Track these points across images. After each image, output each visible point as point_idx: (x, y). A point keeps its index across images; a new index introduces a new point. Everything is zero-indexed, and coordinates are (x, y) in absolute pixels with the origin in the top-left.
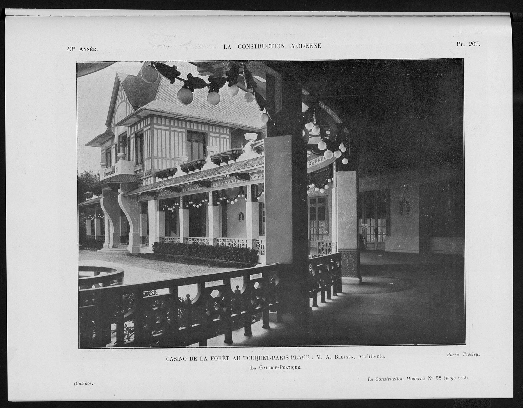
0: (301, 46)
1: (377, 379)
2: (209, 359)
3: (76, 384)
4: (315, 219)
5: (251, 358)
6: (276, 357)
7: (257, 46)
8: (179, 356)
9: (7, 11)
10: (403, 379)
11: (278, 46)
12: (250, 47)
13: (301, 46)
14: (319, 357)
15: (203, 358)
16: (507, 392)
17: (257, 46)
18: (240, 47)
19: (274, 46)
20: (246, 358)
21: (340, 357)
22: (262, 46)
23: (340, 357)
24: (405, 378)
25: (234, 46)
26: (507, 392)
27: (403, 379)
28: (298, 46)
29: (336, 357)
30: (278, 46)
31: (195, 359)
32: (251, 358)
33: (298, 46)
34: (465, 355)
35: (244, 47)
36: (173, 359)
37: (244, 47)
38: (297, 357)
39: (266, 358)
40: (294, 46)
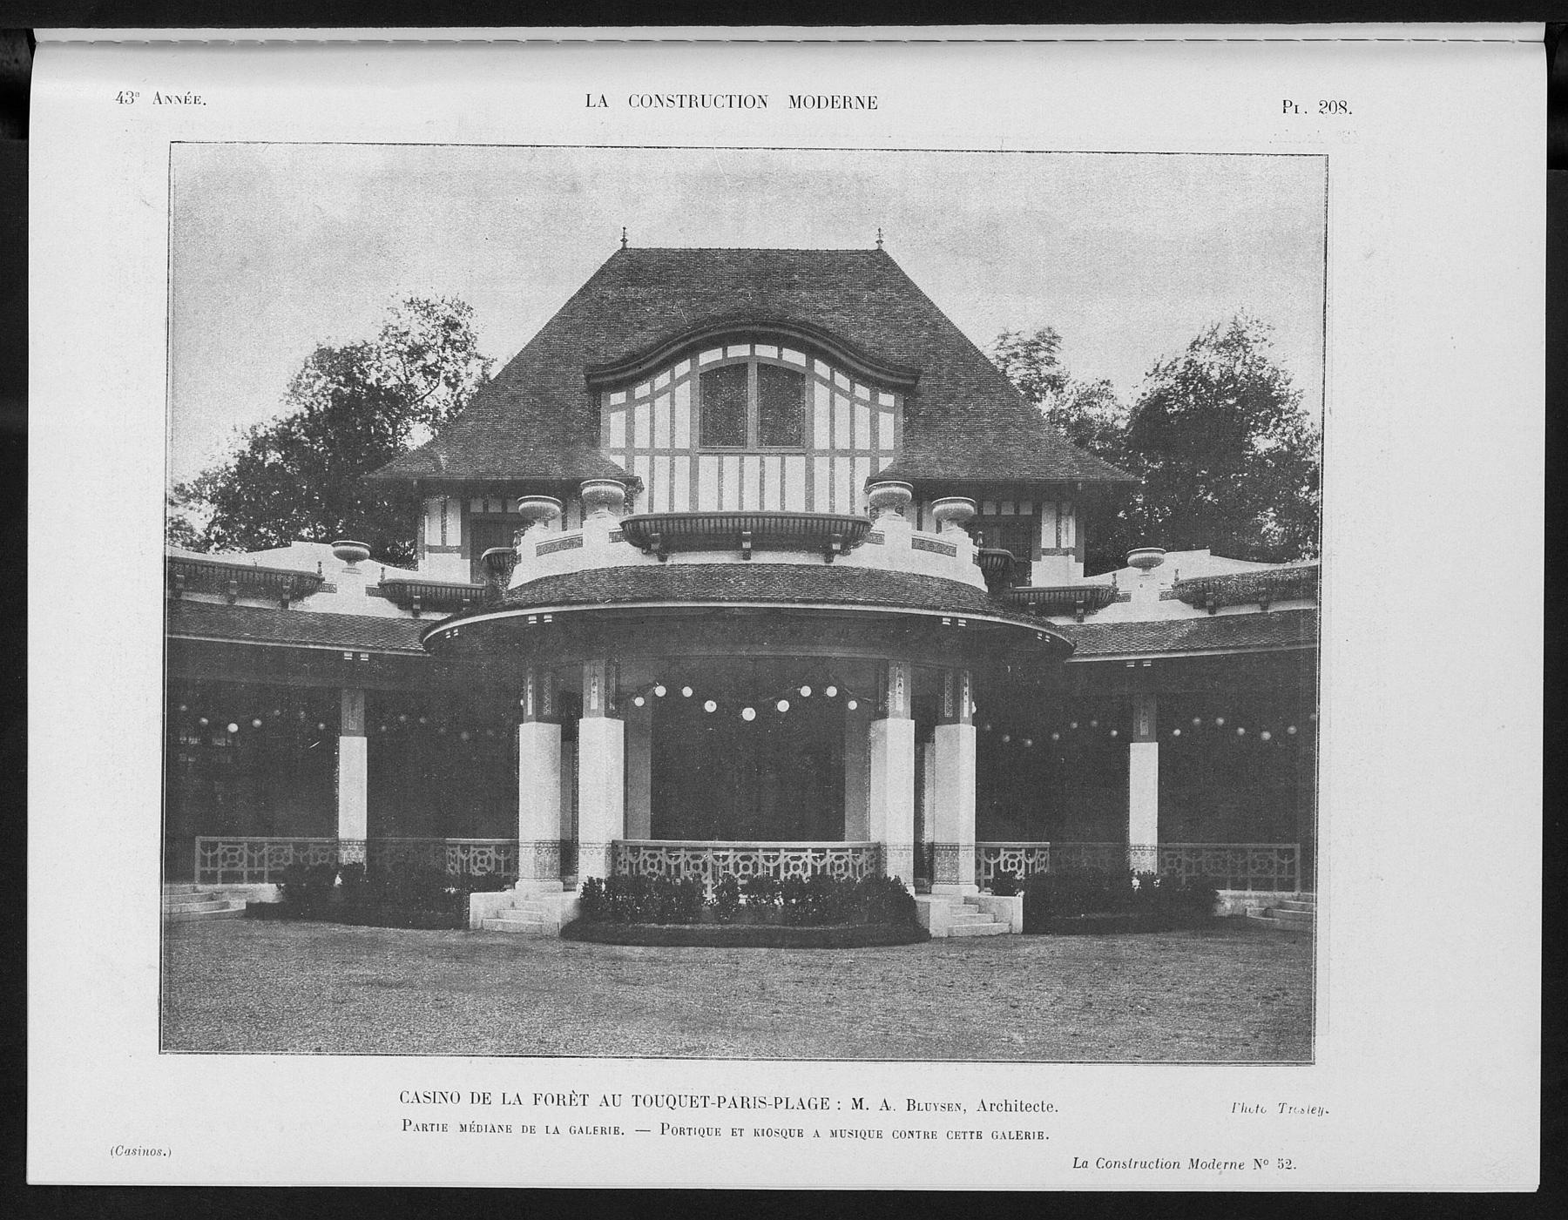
0: (817, 102)
1: (1102, 1163)
3: (115, 1151)
4: (742, 442)
5: (655, 1101)
6: (729, 1100)
7: (686, 101)
9: (41, 34)
10: (1176, 1165)
11: (750, 102)
12: (665, 102)
13: (817, 102)
15: (511, 1097)
16: (1511, 1161)
17: (686, 101)
18: (636, 101)
20: (640, 1101)
21: (923, 1106)
23: (923, 1106)
24: (1185, 1164)
25: (779, 101)
26: (1511, 1161)
27: (1176, 1165)
28: (809, 102)
30: (750, 102)
32: (655, 1101)
33: (809, 102)
34: (1286, 1109)
35: (646, 101)
36: (421, 1098)
37: (646, 101)
38: (794, 1102)
40: (796, 102)
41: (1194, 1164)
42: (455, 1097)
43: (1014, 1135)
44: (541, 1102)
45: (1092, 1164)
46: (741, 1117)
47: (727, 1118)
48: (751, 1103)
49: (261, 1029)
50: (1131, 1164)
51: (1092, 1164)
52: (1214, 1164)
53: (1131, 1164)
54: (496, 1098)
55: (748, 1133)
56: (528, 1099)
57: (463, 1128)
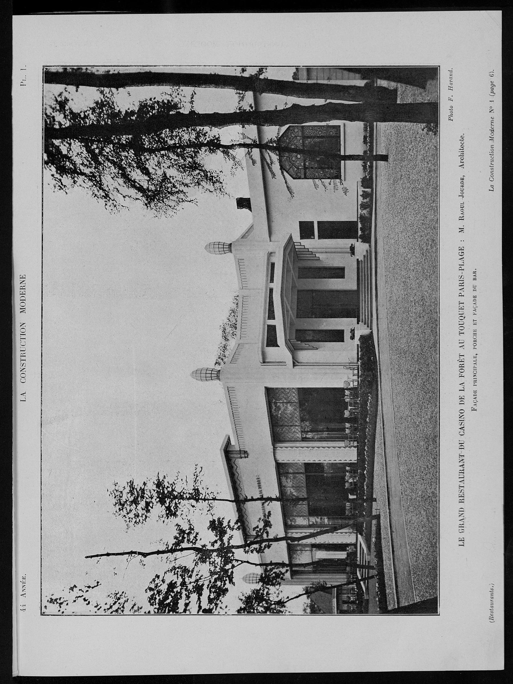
1: (491, 179)
2: (461, 224)
6: (460, 291)
7: (23, 358)
8: (464, 164)
11: (23, 330)
12: (23, 367)
17: (23, 358)
19: (23, 337)
20: (461, 332)
22: (23, 352)
27: (492, 147)
30: (23, 330)
31: (461, 444)
33: (23, 304)
35: (23, 375)
36: (463, 426)
37: (23, 375)
38: (461, 262)
39: (461, 305)
41: (492, 139)
42: (462, 411)
43: (475, 359)
44: (463, 374)
45: (492, 183)
46: (468, 322)
47: (468, 292)
48: (461, 282)
49: (430, 569)
50: (492, 167)
51: (492, 183)
52: (492, 131)
53: (492, 167)
54: (462, 394)
55: (475, 317)
56: (462, 380)
57: (475, 279)
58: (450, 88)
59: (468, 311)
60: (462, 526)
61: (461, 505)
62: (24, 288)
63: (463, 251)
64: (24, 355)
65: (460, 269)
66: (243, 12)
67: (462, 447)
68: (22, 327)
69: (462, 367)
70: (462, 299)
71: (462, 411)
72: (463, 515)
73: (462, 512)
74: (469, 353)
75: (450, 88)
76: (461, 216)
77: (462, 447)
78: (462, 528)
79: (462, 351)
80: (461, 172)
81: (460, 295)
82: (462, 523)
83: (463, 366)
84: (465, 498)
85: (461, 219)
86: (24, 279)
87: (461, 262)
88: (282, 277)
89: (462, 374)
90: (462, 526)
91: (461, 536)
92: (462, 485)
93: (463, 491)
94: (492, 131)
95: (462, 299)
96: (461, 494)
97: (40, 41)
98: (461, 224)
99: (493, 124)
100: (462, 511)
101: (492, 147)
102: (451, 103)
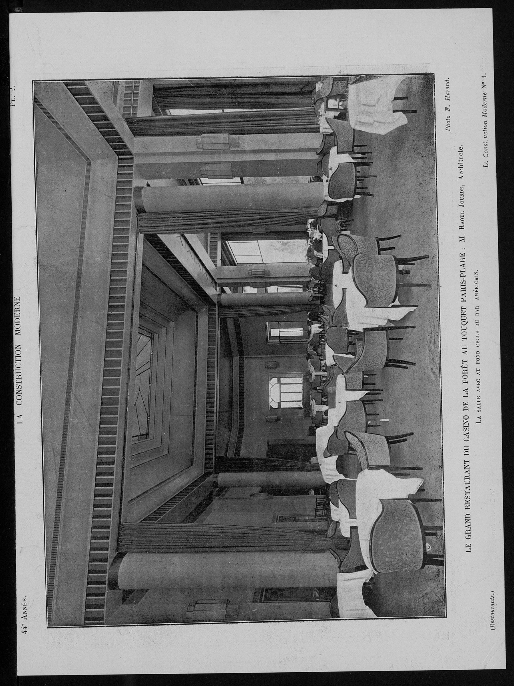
2: (461, 233)
6: (463, 297)
12: (19, 389)
14: (462, 239)
20: (464, 337)
27: (485, 123)
29: (461, 228)
36: (467, 432)
37: (19, 398)
38: (462, 269)
41: (484, 115)
42: (466, 417)
48: (463, 287)
52: (485, 106)
54: (465, 400)
55: (477, 318)
56: (465, 386)
58: (447, 98)
59: (471, 316)
60: (468, 532)
61: (468, 511)
62: (18, 310)
63: (464, 257)
64: (20, 377)
65: (462, 275)
66: (15, 501)
67: (467, 453)
68: (18, 395)
69: (465, 373)
70: (464, 305)
71: (466, 417)
72: (469, 522)
73: (469, 519)
74: (470, 357)
75: (447, 98)
76: (462, 225)
77: (467, 453)
78: (469, 534)
79: (465, 357)
80: (460, 183)
81: (462, 300)
82: (468, 529)
83: (466, 372)
84: (471, 504)
85: (461, 228)
86: (18, 301)
87: (462, 269)
88: (314, 132)
89: (465, 380)
90: (468, 532)
91: (468, 542)
92: (468, 491)
93: (469, 497)
94: (485, 106)
95: (464, 305)
96: (467, 500)
97: (46, 47)
98: (461, 233)
99: (485, 100)
100: (468, 518)
101: (485, 123)
102: (447, 113)
